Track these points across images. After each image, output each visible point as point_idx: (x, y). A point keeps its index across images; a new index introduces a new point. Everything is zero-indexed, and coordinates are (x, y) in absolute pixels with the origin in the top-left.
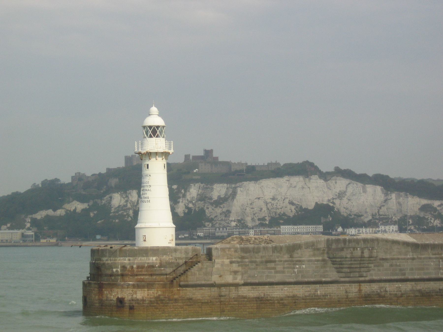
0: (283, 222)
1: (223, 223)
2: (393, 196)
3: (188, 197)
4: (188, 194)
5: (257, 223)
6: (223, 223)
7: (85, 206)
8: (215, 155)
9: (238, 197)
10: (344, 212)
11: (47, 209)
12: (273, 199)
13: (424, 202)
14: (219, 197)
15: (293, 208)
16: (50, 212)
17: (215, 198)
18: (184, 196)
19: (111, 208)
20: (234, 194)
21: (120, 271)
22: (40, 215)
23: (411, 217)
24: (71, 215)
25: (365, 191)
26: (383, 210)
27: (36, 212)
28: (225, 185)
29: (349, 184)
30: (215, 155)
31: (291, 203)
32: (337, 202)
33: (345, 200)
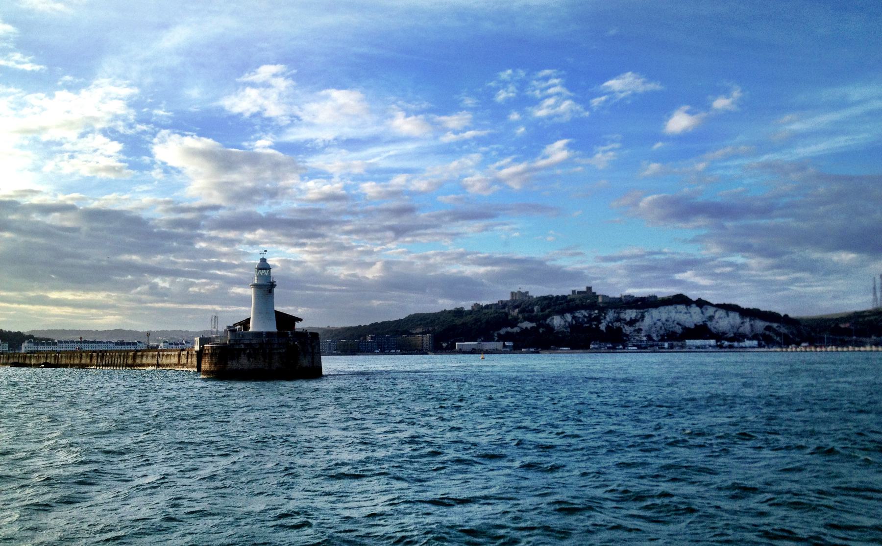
0: (602, 331)
1: (637, 338)
2: (748, 320)
3: (608, 319)
4: (607, 316)
5: (660, 338)
6: (637, 338)
7: (534, 325)
8: (593, 291)
9: (646, 319)
10: (714, 330)
11: (506, 327)
12: (667, 321)
13: (767, 324)
14: (631, 318)
15: (680, 327)
16: (509, 329)
17: (628, 319)
18: (605, 318)
19: (380, 193)
20: (643, 317)
21: (371, 163)
22: (503, 331)
23: (761, 335)
24: (525, 331)
25: (728, 316)
26: (741, 330)
27: (500, 329)
28: (635, 311)
29: (716, 311)
30: (593, 291)
31: (678, 324)
32: (709, 323)
33: (714, 322)
